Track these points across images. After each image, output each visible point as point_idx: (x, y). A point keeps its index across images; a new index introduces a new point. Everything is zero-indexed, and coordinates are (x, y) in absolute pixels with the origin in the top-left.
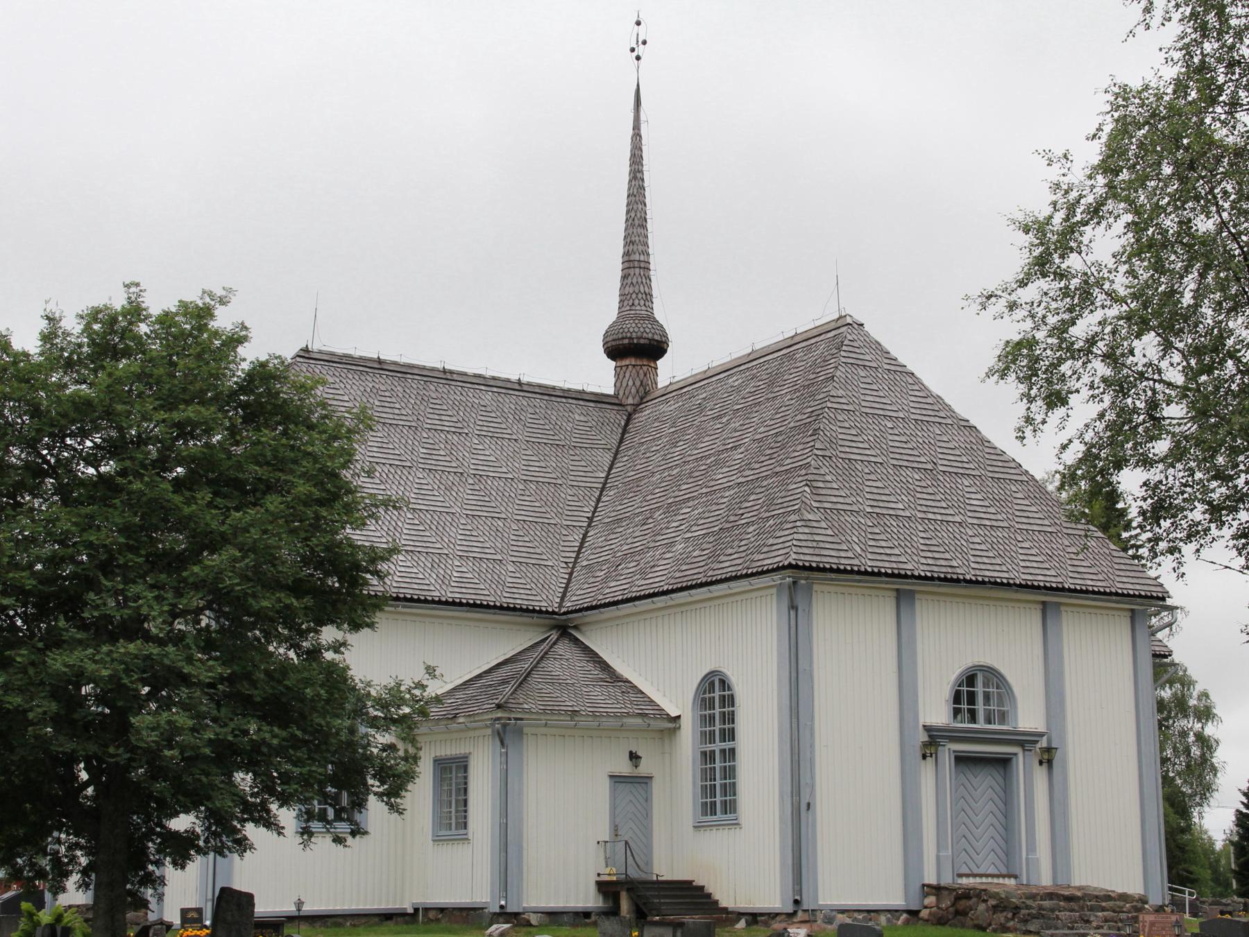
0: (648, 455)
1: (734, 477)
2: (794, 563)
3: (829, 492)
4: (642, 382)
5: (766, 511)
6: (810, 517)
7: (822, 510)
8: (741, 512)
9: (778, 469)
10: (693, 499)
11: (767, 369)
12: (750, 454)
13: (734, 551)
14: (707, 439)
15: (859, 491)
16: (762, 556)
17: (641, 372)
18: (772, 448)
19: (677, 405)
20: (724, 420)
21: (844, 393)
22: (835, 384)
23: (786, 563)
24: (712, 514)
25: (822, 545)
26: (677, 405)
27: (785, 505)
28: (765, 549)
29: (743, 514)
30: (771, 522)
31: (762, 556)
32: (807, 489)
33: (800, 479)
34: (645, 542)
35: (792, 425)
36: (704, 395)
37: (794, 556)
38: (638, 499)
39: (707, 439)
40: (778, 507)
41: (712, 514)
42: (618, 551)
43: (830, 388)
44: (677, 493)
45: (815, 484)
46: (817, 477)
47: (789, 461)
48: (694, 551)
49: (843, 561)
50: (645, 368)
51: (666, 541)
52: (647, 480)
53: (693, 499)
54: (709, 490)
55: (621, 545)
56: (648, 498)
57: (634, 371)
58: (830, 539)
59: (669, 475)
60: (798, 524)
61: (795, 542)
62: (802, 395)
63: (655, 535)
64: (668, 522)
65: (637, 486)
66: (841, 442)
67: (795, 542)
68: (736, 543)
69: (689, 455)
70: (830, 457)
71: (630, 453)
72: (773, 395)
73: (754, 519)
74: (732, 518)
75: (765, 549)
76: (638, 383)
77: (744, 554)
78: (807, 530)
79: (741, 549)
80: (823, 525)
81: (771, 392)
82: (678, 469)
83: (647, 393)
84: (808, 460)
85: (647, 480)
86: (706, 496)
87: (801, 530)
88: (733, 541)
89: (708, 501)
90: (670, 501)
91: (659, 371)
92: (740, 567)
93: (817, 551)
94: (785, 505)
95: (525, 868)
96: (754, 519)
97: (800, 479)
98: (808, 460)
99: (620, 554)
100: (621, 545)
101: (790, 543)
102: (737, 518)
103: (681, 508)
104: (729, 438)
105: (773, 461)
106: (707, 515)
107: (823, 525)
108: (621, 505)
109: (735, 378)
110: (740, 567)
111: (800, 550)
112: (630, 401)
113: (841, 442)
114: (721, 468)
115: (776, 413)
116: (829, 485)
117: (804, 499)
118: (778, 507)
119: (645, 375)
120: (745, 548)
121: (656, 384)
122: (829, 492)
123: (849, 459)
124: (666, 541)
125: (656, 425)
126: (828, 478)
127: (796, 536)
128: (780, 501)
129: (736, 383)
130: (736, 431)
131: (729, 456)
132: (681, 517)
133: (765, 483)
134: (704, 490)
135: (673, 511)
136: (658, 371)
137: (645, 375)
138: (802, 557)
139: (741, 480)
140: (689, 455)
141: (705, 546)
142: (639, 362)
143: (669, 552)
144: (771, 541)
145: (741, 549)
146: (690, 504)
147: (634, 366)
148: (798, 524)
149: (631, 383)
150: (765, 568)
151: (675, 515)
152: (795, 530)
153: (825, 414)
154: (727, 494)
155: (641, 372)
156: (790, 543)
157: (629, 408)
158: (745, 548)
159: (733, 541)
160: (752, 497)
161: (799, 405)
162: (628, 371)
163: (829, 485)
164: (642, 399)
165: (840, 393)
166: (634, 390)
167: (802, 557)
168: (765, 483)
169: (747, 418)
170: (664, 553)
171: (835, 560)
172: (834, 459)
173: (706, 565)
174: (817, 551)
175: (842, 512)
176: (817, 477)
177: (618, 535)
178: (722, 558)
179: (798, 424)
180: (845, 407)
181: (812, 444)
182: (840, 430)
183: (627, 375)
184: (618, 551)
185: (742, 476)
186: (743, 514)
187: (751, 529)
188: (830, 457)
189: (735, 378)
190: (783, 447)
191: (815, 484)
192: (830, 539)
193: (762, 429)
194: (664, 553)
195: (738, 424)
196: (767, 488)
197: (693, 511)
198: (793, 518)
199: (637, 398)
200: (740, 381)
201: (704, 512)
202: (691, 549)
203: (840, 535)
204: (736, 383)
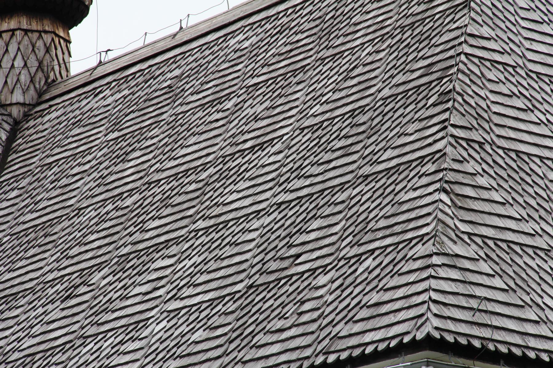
0: (64, 181)
1: (268, 195)
2: (436, 335)
3: (487, 207)
4: (40, 63)
5: (351, 245)
6: (458, 249)
7: (479, 240)
8: (293, 251)
9: (367, 170)
10: (177, 241)
11: (310, 13)
12: (297, 152)
13: (288, 323)
14: (193, 140)
15: (543, 213)
16: (357, 328)
17: (40, 44)
18: (346, 137)
19: (118, 96)
20: (229, 105)
21: (493, 34)
22: (473, 14)
23: (420, 336)
24: (226, 263)
25: (491, 307)
26: (118, 96)
27: (397, 229)
28: (364, 313)
29: (298, 256)
30: (369, 263)
31: (357, 328)
32: (444, 197)
33: (425, 180)
34: (75, 327)
35: (386, 92)
36: (177, 72)
37: (436, 322)
38: (50, 257)
39: (193, 140)
40: (380, 234)
41: (226, 263)
42: (13, 350)
43: (466, 20)
44: (138, 236)
45: (458, 189)
46: (460, 178)
47: (389, 154)
48: (193, 331)
49: (533, 343)
50: (48, 38)
51: (123, 322)
52: (66, 223)
53: (177, 241)
54: (212, 222)
55: (19, 340)
56: (72, 252)
57: (26, 41)
58: (500, 296)
59: (117, 209)
60: (436, 260)
61: (434, 296)
62: (401, 41)
63: (96, 314)
64: (125, 287)
65: (46, 236)
66: (497, 119)
67: (434, 296)
68: (291, 308)
69: (158, 171)
70: (480, 144)
71: (24, 183)
72: (331, 52)
73: (328, 260)
74: (274, 266)
75: (364, 313)
76: (33, 63)
77: (313, 327)
78: (454, 274)
79: (305, 318)
80: (484, 267)
81: (327, 48)
82: (136, 197)
83: (50, 84)
84: (439, 146)
85: (66, 223)
86: (207, 234)
87: (443, 272)
88: (283, 305)
89: (212, 241)
90: (125, 251)
91: (73, 47)
92: (308, 352)
93: (480, 318)
94: (397, 229)
95: (350, 283)
96: (328, 260)
97: (425, 180)
98: (439, 146)
99: (16, 355)
100: (19, 340)
101: (424, 297)
102: (286, 264)
103: (153, 261)
104: (242, 133)
105: (355, 157)
106: (213, 265)
107: (484, 267)
108: (10, 271)
109: (241, 37)
110: (308, 352)
111: (447, 312)
112: (18, 97)
113: (497, 119)
114: (235, 183)
115: (345, 79)
116: (485, 195)
117: (441, 216)
118: (380, 234)
119: (48, 50)
120: (316, 314)
121: (67, 70)
122: (487, 207)
123: (517, 152)
124: (123, 322)
125: (77, 131)
126: (482, 181)
127: (434, 283)
128: (383, 223)
129: (247, 44)
130: (256, 119)
131: (249, 162)
132: (154, 276)
133: (343, 196)
134: (201, 224)
135: (133, 267)
136: (72, 47)
137: (48, 50)
138: (451, 326)
139: (282, 197)
140: (158, 171)
141: (216, 321)
142: (35, 26)
143: (132, 339)
144: (375, 298)
145: (305, 318)
146: (174, 250)
147: (26, 31)
148: (436, 260)
149: (19, 63)
150: (369, 350)
151: (139, 274)
152: (431, 271)
153: (461, 66)
154: (256, 224)
155: (40, 44)
156: (424, 297)
157: (15, 111)
158: (316, 314)
159: (283, 305)
160: (315, 224)
161: (397, 58)
162: (14, 40)
163: (485, 195)
164: (40, 94)
165: (485, 31)
166: (24, 78)
167: (451, 326)
168: (343, 196)
169: (280, 96)
170: (121, 343)
171: (517, 339)
172: (487, 147)
173: (226, 354)
174: (480, 318)
175: (517, 249)
176: (460, 178)
177: (11, 322)
178: (261, 339)
179: (401, 89)
180: (497, 57)
181: (446, 115)
182: (493, 97)
183: (13, 48)
184: (13, 350)
185: (285, 191)
186: (298, 256)
187: (322, 280)
188: (480, 144)
189: (241, 37)
190: (373, 131)
191: (458, 189)
192: (500, 296)
193: (318, 109)
194: (121, 343)
195: (259, 108)
196: (348, 204)
197: (179, 261)
198: (420, 250)
199: (32, 92)
200: (254, 39)
201: (205, 262)
202: (184, 328)
203: (519, 291)
204: (247, 44)
